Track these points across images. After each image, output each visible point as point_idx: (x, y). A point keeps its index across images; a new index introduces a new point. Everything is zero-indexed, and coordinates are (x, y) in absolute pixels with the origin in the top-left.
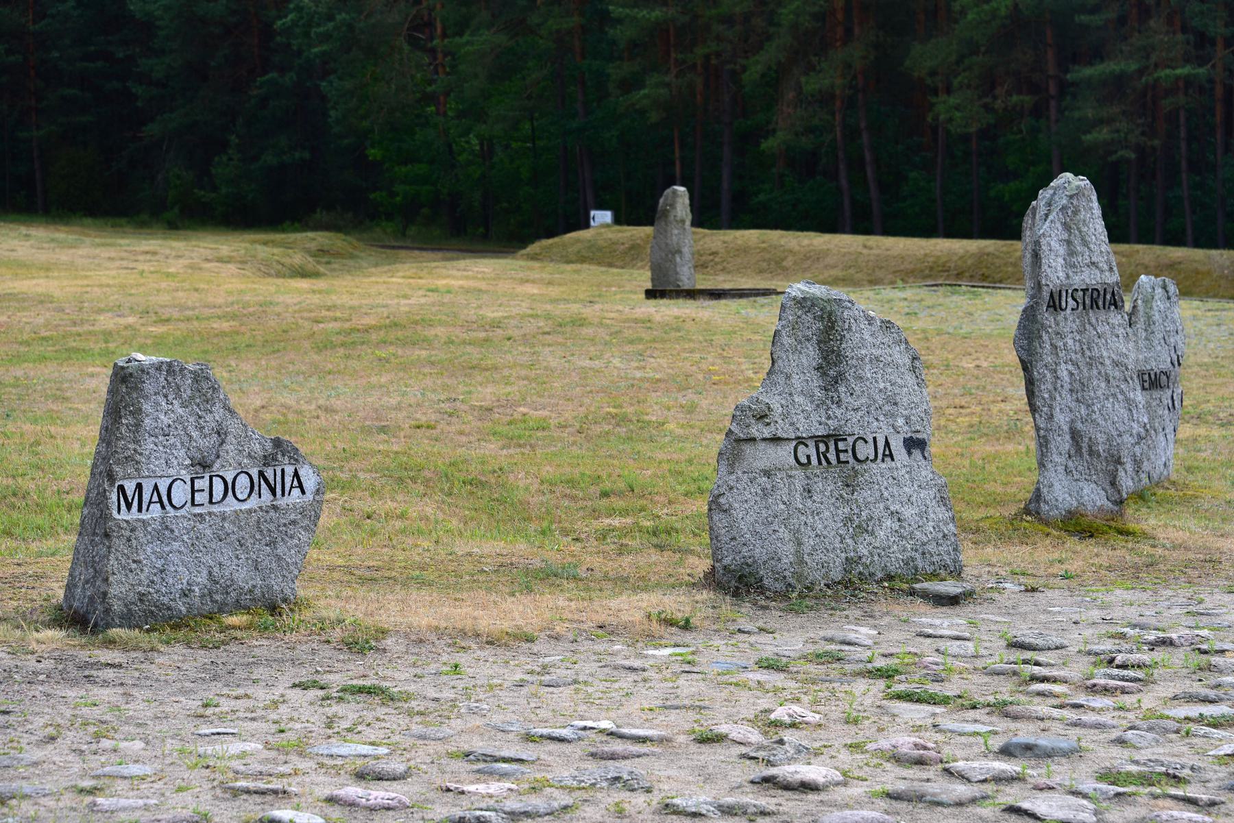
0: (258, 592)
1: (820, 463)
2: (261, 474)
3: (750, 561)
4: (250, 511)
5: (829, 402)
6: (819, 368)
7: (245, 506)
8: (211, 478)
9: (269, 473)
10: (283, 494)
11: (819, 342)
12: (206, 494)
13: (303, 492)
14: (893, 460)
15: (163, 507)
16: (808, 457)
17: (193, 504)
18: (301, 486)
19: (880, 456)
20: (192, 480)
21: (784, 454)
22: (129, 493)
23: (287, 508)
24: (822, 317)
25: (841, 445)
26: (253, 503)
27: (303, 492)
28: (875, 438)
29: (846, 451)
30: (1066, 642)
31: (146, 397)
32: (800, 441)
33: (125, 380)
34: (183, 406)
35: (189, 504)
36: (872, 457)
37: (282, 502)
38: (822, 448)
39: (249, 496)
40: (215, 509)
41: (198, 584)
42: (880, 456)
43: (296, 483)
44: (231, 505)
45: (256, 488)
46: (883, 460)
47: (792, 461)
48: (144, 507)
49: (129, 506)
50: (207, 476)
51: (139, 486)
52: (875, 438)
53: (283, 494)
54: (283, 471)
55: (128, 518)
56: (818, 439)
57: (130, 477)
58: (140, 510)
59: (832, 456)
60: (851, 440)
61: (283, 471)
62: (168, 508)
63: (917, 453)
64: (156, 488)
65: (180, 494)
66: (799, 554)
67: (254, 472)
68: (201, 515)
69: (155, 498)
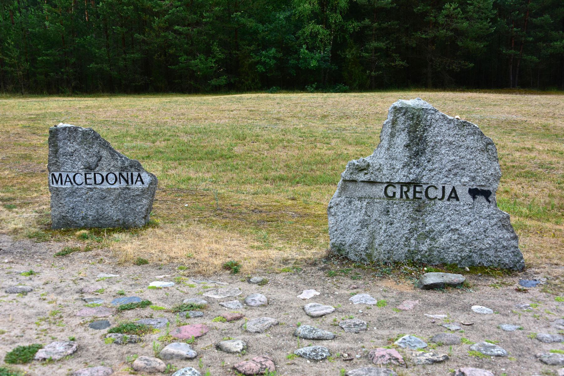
0: (121, 222)
1: (401, 197)
2: (120, 174)
3: (343, 243)
4: (115, 189)
5: (411, 165)
6: (407, 146)
7: (112, 187)
8: (95, 174)
9: (125, 174)
10: (132, 183)
11: (409, 132)
12: (93, 180)
13: (143, 183)
14: (458, 199)
15: (72, 183)
16: (394, 193)
17: (86, 183)
18: (142, 180)
19: (446, 197)
20: (85, 174)
21: (378, 191)
22: (57, 177)
23: (134, 190)
24: (412, 118)
25: (418, 189)
26: (117, 185)
27: (143, 183)
28: (444, 187)
29: (421, 192)
30: (149, 296)
31: (60, 141)
32: (390, 184)
33: (54, 133)
34: (78, 144)
35: (84, 183)
36: (440, 196)
37: (134, 186)
38: (405, 189)
39: (115, 182)
40: (98, 186)
41: (90, 215)
42: (446, 197)
43: (139, 179)
44: (105, 186)
45: (118, 180)
46: (448, 200)
47: (382, 194)
48: (63, 183)
49: (57, 182)
50: (93, 174)
51: (60, 175)
52: (444, 187)
53: (132, 183)
54: (132, 174)
55: (57, 186)
56: (402, 184)
57: (56, 171)
58: (62, 184)
59: (410, 195)
60: (425, 187)
61: (132, 174)
62: (74, 184)
63: (481, 199)
64: (68, 176)
65: (79, 179)
66: (371, 244)
67: (117, 173)
68: (90, 188)
69: (68, 180)
